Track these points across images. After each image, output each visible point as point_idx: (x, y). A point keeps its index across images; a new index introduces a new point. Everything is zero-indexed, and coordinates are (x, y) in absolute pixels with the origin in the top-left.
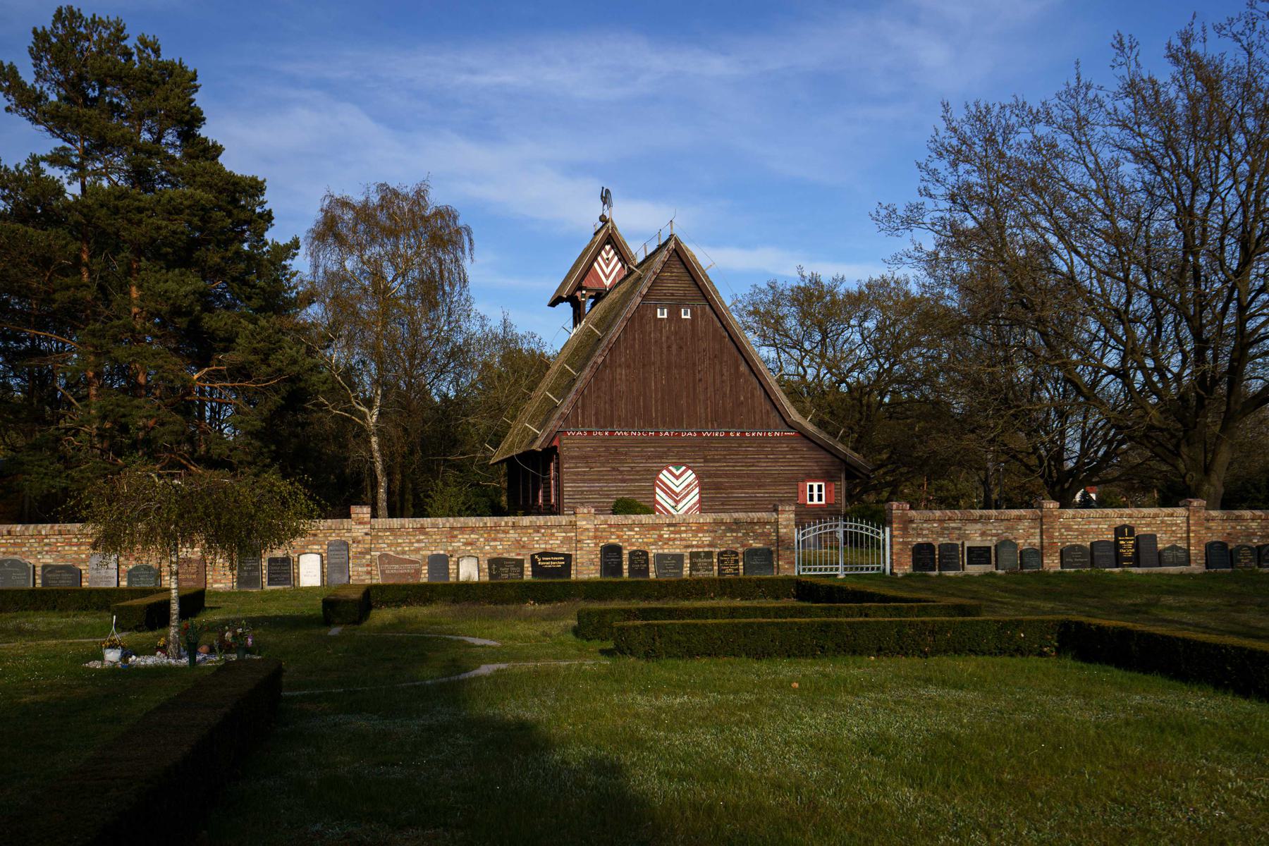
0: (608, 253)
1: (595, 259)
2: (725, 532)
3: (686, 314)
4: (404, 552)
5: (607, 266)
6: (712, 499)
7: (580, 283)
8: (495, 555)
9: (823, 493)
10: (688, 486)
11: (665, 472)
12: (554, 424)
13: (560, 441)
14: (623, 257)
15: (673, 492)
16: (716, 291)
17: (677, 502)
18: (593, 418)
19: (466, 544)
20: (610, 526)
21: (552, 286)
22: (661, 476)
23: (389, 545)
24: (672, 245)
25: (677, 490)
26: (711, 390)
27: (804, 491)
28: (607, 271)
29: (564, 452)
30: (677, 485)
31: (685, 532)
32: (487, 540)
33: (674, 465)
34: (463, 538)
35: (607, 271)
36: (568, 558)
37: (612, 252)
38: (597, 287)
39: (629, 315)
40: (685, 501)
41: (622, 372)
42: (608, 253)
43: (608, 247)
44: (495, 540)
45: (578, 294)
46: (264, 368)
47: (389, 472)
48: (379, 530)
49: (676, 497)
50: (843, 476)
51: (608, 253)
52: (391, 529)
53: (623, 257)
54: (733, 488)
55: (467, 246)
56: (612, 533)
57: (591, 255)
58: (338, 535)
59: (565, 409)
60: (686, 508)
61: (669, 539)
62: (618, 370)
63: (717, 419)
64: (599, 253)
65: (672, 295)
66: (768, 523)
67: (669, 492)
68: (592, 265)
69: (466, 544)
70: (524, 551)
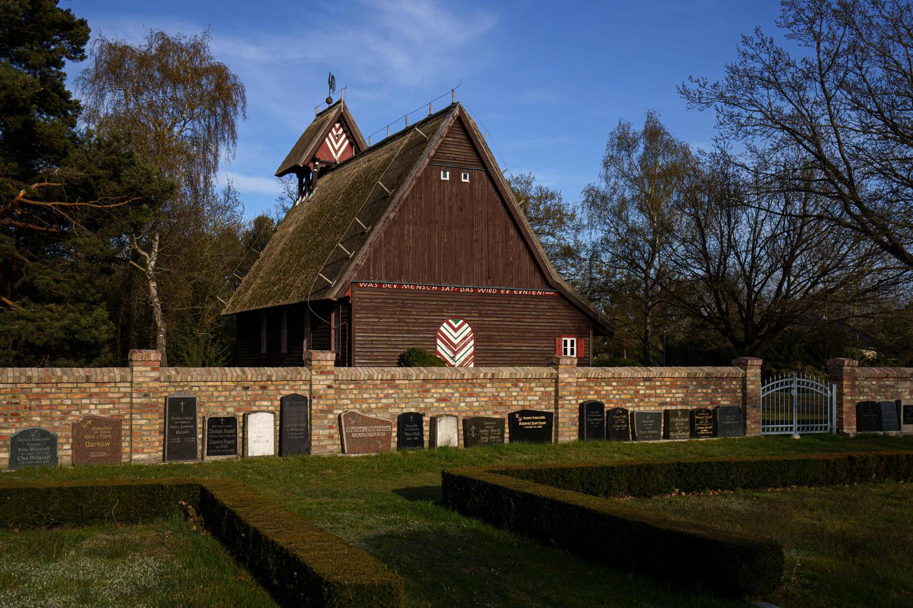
2: (697, 387)
3: (465, 177)
4: (370, 410)
5: (337, 142)
6: (484, 351)
8: (471, 414)
10: (465, 338)
11: (445, 325)
12: (350, 275)
15: (452, 343)
16: (493, 158)
17: (455, 353)
18: (383, 271)
19: (440, 400)
20: (589, 379)
22: (442, 329)
23: (353, 401)
24: (456, 112)
25: (456, 342)
27: (560, 346)
28: (337, 147)
29: (355, 303)
30: (457, 338)
31: (660, 387)
32: (462, 395)
33: (453, 318)
34: (436, 392)
35: (337, 147)
36: (549, 416)
37: (341, 130)
38: (327, 160)
39: (419, 175)
40: (462, 353)
42: (337, 130)
43: (337, 125)
44: (471, 395)
45: (311, 165)
46: (114, 185)
48: (342, 382)
49: (455, 349)
50: (591, 332)
51: (337, 130)
52: (355, 381)
54: (502, 341)
56: (590, 388)
58: (293, 388)
59: (360, 260)
60: (462, 359)
61: (645, 396)
62: (406, 227)
63: (490, 277)
65: (454, 159)
66: (733, 379)
67: (449, 344)
69: (440, 400)
70: (502, 409)
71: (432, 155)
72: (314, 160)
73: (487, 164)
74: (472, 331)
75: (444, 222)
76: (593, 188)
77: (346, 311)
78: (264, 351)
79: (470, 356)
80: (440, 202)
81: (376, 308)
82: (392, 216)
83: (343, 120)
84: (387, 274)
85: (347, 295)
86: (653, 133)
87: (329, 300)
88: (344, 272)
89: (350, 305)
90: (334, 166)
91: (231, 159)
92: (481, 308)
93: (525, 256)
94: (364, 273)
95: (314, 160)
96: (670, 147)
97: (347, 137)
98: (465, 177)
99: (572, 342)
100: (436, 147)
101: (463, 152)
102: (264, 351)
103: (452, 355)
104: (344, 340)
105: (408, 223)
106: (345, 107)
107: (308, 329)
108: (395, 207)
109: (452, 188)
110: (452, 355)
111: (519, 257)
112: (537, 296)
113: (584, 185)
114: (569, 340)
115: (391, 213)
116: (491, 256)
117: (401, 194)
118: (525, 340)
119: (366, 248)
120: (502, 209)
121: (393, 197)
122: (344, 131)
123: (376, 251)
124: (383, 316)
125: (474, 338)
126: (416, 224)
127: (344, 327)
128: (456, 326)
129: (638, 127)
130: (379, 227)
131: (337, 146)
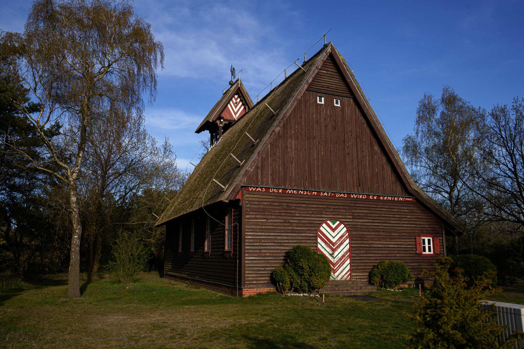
0: (236, 99)
1: (229, 103)
3: (337, 103)
7: (220, 115)
9: (432, 245)
10: (341, 237)
11: (324, 225)
12: (240, 179)
13: (243, 195)
14: (245, 101)
17: (334, 250)
21: (199, 121)
22: (321, 228)
24: (329, 49)
25: (334, 240)
26: (355, 161)
28: (236, 110)
29: (245, 205)
35: (236, 110)
37: (239, 100)
39: (299, 97)
40: (339, 250)
41: (292, 143)
42: (236, 99)
43: (236, 96)
45: (218, 122)
47: (84, 223)
49: (333, 247)
50: (444, 232)
53: (245, 101)
54: (373, 239)
55: (159, 56)
57: (227, 98)
60: (340, 255)
62: (289, 140)
64: (231, 99)
67: (328, 242)
68: (227, 105)
71: (310, 81)
72: (220, 118)
73: (354, 92)
74: (347, 231)
75: (321, 138)
76: (410, 138)
77: (237, 213)
78: (180, 251)
79: (346, 252)
80: (317, 121)
81: (264, 210)
82: (277, 129)
83: (240, 92)
84: (273, 180)
85: (237, 198)
86: (450, 100)
87: (221, 201)
88: (235, 178)
89: (241, 207)
90: (234, 123)
91: (153, 101)
92: (354, 211)
93: (388, 169)
94: (253, 179)
95: (220, 118)
96: (460, 111)
97: (243, 104)
98: (337, 103)
99: (429, 240)
100: (313, 76)
101: (335, 82)
102: (180, 251)
103: (331, 252)
104: (235, 239)
105: (291, 138)
106: (241, 84)
107: (208, 232)
108: (280, 122)
109: (326, 111)
110: (331, 252)
111: (383, 169)
112: (399, 201)
113: (404, 136)
114: (426, 239)
115: (276, 128)
116: (360, 167)
117: (284, 112)
118: (392, 238)
119: (255, 156)
120: (368, 130)
121: (277, 115)
122: (241, 100)
123: (263, 160)
124: (270, 217)
125: (349, 237)
126: (298, 138)
127: (235, 227)
128: (334, 227)
129: (437, 97)
130: (266, 138)
131: (236, 109)
